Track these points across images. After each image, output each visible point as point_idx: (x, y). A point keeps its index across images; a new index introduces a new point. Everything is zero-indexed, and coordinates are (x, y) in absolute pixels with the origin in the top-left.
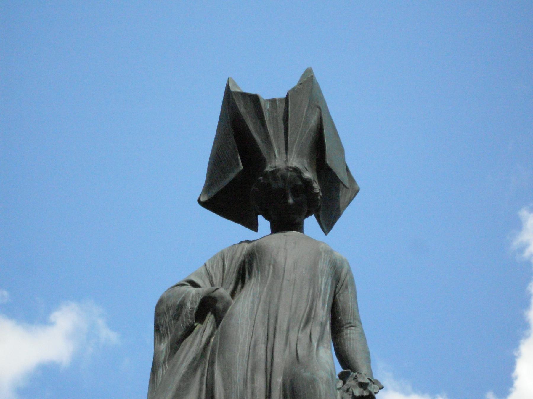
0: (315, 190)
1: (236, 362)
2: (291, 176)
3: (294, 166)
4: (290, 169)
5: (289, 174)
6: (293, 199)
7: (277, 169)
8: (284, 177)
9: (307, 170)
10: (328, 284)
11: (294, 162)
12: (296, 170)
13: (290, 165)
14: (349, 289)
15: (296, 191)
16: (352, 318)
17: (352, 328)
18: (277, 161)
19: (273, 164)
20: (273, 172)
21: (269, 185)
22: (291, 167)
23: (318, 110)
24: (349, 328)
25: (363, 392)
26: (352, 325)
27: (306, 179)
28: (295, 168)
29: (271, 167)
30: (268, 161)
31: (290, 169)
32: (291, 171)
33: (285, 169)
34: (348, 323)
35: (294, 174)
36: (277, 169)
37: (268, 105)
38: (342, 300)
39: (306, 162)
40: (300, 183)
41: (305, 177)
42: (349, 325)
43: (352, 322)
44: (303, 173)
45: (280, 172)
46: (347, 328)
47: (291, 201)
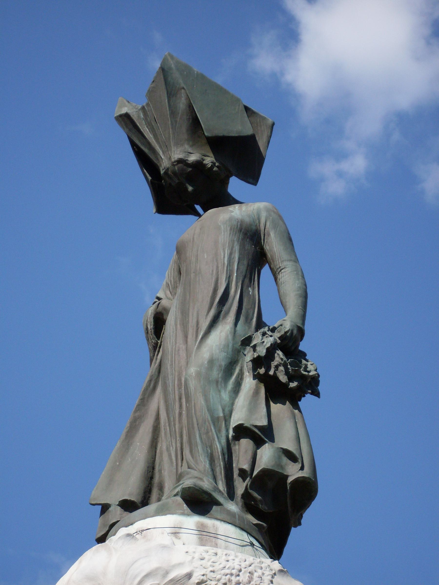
0: (207, 166)
1: (169, 373)
2: (178, 169)
3: (176, 159)
4: (175, 164)
5: (176, 168)
6: (192, 186)
7: (166, 169)
8: (174, 173)
9: (192, 153)
10: (235, 251)
11: (177, 155)
12: (180, 161)
13: (173, 160)
14: (271, 235)
15: (190, 179)
16: (280, 261)
17: (282, 271)
18: (164, 161)
19: (163, 166)
20: (166, 173)
21: (170, 184)
22: (175, 162)
23: (183, 91)
24: (280, 273)
25: (253, 354)
26: (281, 268)
27: (192, 163)
28: (178, 159)
29: (163, 170)
30: (159, 165)
31: (175, 164)
32: (177, 164)
33: (172, 165)
34: (278, 269)
35: (180, 165)
36: (166, 169)
37: (142, 114)
38: (268, 249)
39: (187, 147)
40: (190, 169)
41: (192, 161)
42: (279, 270)
43: (281, 265)
44: (187, 160)
45: (169, 170)
46: (279, 273)
47: (190, 188)
